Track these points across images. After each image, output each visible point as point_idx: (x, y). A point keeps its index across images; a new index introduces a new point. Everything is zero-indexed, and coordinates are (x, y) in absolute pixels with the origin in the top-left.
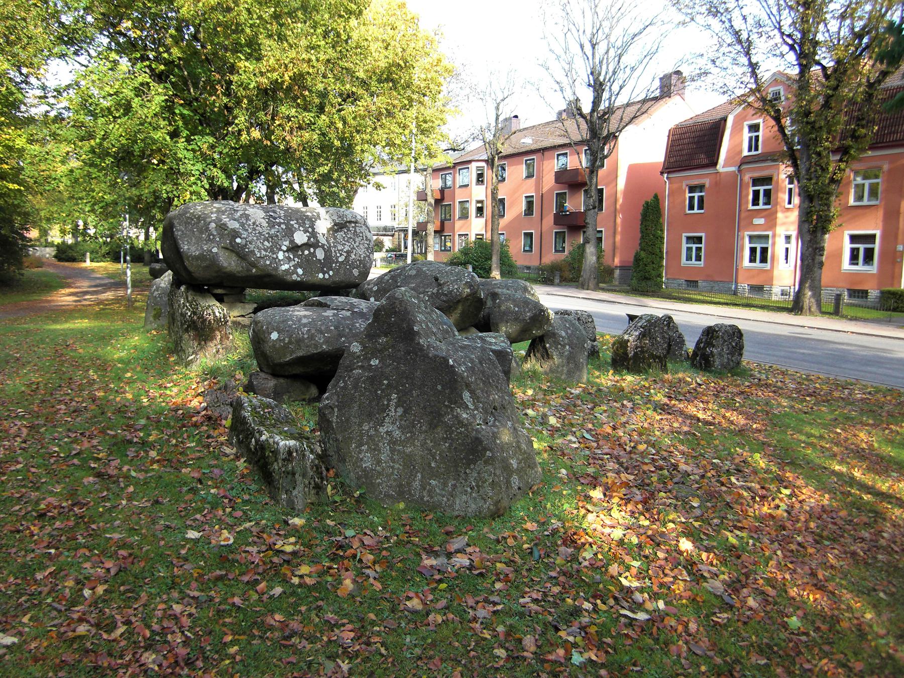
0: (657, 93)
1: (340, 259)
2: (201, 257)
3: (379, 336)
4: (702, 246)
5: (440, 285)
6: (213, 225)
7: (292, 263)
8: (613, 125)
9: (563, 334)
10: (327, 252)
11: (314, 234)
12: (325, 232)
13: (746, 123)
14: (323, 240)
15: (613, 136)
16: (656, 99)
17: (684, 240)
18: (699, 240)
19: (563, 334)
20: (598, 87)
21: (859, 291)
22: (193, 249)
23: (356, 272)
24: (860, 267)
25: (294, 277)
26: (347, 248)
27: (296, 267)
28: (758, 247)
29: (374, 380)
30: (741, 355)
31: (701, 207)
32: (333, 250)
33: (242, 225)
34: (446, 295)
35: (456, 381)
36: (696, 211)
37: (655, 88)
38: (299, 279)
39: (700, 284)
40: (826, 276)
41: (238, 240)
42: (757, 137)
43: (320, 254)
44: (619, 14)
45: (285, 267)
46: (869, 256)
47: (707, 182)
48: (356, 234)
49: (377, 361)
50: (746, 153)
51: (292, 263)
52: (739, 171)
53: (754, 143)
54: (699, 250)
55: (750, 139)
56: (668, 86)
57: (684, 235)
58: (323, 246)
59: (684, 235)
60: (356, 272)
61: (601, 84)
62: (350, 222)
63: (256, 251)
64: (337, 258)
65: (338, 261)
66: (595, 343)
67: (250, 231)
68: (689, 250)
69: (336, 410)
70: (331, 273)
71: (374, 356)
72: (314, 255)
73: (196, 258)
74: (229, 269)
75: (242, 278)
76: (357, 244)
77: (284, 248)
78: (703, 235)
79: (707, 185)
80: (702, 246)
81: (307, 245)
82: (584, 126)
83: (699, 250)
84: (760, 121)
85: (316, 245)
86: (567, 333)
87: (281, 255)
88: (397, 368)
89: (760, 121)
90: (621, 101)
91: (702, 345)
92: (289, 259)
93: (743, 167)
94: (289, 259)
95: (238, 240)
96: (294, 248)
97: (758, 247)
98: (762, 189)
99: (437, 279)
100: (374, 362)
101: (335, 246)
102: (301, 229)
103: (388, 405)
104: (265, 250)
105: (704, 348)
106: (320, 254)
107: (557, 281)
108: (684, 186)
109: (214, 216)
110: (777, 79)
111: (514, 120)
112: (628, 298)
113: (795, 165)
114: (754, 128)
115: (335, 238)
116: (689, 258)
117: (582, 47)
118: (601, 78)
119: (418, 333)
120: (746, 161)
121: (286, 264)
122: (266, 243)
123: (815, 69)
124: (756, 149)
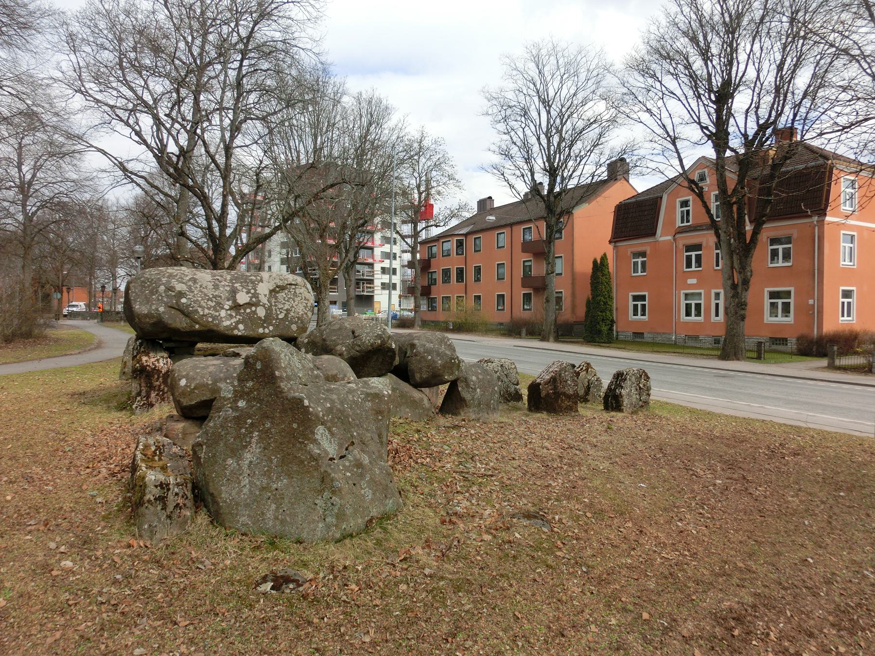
0: (605, 176)
1: (280, 317)
2: (149, 315)
3: (247, 380)
4: (646, 303)
5: (355, 337)
6: (162, 288)
7: (234, 320)
8: (563, 205)
9: (474, 378)
10: (269, 310)
11: (255, 295)
12: (267, 293)
13: (678, 200)
14: (264, 300)
15: (569, 212)
16: (604, 182)
17: (766, 295)
18: (643, 298)
19: (474, 378)
20: (552, 172)
21: (780, 339)
22: (143, 308)
23: (294, 327)
24: (780, 319)
25: (236, 332)
26: (286, 307)
27: (238, 323)
28: (693, 303)
29: (239, 421)
30: (649, 395)
31: (644, 269)
32: (274, 308)
33: (190, 287)
34: (359, 346)
35: (310, 420)
36: (640, 274)
37: (603, 173)
38: (240, 334)
39: (645, 336)
40: (747, 327)
41: (184, 300)
42: (688, 211)
43: (261, 312)
44: (568, 113)
45: (227, 323)
46: (786, 308)
47: (648, 249)
48: (295, 295)
49: (244, 403)
50: (679, 224)
51: (234, 320)
52: (675, 240)
53: (685, 216)
54: (644, 306)
55: (682, 212)
56: (618, 169)
57: (766, 290)
58: (264, 306)
59: (766, 290)
60: (294, 327)
61: (555, 170)
62: (291, 284)
63: (200, 310)
64: (277, 315)
65: (278, 318)
66: (518, 387)
67: (196, 292)
68: (636, 307)
69: (204, 447)
70: (271, 328)
71: (241, 397)
72: (255, 312)
73: (146, 316)
74: (173, 326)
75: (186, 332)
76: (296, 303)
77: (227, 307)
78: (646, 293)
79: (648, 252)
80: (646, 303)
81: (249, 304)
82: (542, 205)
83: (644, 306)
84: (690, 198)
85: (257, 304)
86: (478, 378)
87: (223, 313)
88: (260, 408)
89: (690, 198)
90: (572, 184)
91: (613, 387)
92: (231, 316)
93: (677, 236)
94: (231, 316)
95: (184, 300)
96: (236, 307)
97: (693, 303)
98: (693, 254)
99: (353, 332)
100: (241, 404)
101: (276, 306)
102: (245, 290)
103: (250, 443)
104: (209, 309)
105: (615, 389)
106: (261, 312)
107: (523, 334)
108: (629, 253)
109: (164, 280)
110: (702, 161)
111: (488, 201)
112: (19, 361)
113: (718, 236)
114: (685, 204)
115: (276, 298)
116: (635, 314)
117: (538, 139)
118: (556, 164)
119: (281, 377)
120: (682, 231)
121: (226, 320)
122: (210, 303)
123: (728, 153)
124: (688, 221)
